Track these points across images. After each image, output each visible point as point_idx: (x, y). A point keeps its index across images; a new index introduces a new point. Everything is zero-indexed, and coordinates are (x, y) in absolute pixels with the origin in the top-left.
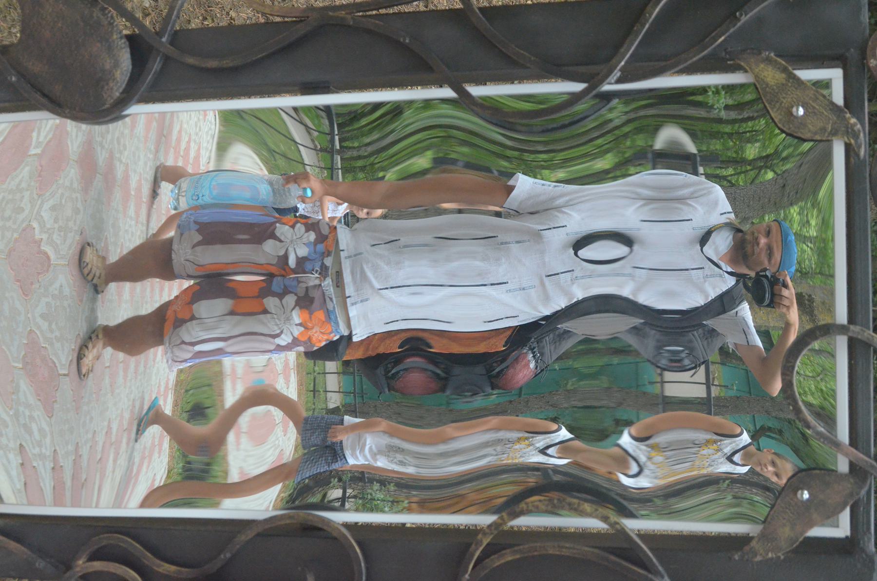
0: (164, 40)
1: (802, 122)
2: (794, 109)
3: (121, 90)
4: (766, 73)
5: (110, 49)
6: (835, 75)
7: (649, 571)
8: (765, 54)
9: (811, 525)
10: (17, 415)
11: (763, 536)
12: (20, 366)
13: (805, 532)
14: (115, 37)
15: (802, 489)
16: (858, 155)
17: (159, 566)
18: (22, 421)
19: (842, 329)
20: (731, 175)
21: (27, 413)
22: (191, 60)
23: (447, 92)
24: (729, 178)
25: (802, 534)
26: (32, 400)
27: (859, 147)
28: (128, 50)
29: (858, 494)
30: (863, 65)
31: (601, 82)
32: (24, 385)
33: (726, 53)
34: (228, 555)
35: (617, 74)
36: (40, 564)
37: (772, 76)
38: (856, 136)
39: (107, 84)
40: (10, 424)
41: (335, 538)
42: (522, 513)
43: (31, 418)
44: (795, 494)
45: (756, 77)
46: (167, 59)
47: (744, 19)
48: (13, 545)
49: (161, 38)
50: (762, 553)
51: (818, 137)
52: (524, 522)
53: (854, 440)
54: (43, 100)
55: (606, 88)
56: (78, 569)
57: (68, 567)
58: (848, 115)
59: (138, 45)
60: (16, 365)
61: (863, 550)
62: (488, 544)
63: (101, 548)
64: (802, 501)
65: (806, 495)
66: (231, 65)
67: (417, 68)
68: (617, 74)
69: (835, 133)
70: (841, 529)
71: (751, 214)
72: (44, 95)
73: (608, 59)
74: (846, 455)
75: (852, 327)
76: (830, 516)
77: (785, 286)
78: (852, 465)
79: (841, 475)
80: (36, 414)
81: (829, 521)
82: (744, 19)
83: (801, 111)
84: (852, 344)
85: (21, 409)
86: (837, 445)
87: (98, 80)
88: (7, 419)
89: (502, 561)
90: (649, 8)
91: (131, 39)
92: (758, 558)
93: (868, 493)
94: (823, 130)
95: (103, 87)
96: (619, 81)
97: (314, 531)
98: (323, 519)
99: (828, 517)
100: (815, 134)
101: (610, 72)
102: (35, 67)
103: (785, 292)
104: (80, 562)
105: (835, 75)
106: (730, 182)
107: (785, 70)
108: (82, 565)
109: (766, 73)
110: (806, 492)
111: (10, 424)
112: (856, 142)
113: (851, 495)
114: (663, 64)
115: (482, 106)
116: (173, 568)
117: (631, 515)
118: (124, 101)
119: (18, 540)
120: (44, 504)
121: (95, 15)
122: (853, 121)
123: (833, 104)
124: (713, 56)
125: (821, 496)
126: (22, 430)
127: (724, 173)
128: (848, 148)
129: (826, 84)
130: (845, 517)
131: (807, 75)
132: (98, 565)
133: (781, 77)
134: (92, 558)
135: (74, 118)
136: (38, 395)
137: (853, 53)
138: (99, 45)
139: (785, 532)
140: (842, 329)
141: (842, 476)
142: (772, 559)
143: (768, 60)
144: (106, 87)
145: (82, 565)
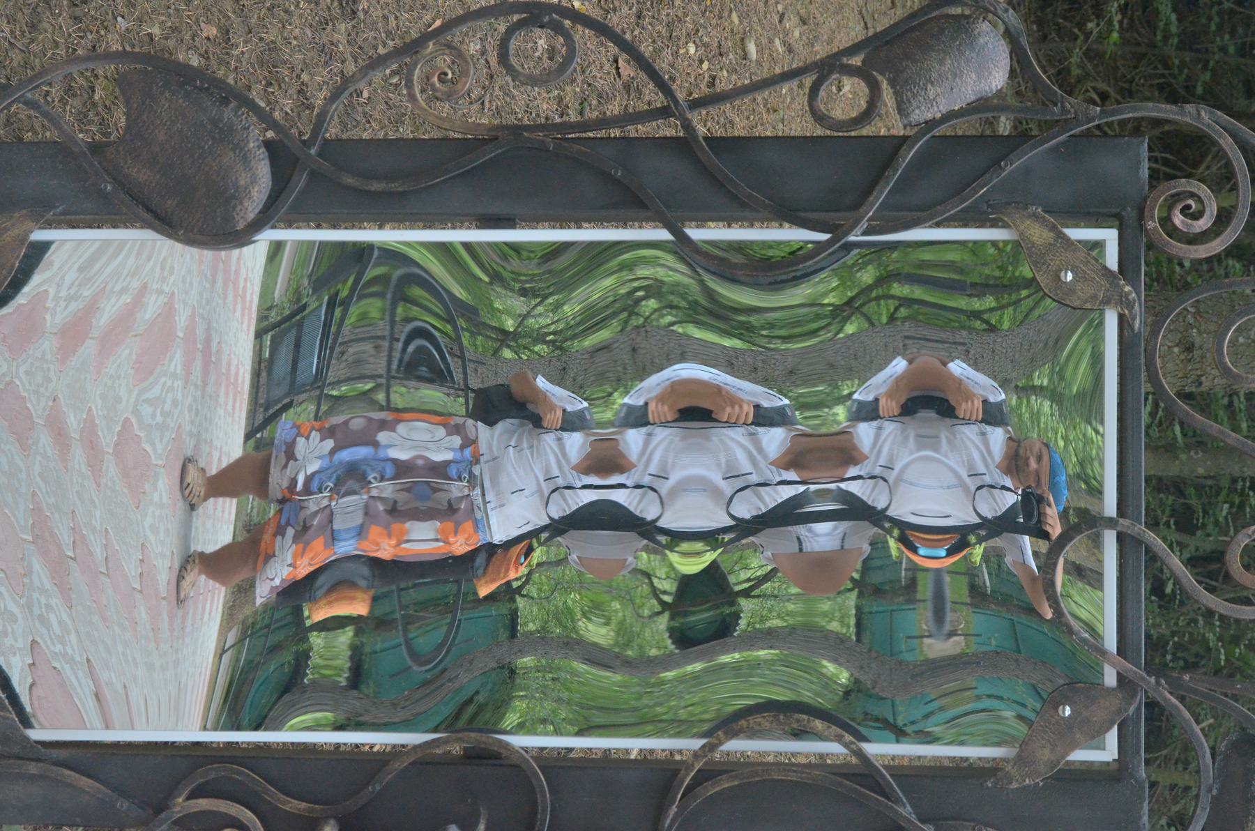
0: (313, 151)
1: (1070, 289)
2: (1063, 274)
3: (257, 211)
4: (1032, 231)
5: (245, 160)
6: (1109, 236)
7: (889, 799)
8: (1032, 209)
9: (1074, 746)
10: (29, 607)
11: (1020, 760)
12: (31, 539)
13: (1067, 754)
14: (252, 145)
15: (1064, 705)
16: (1132, 329)
17: (284, 803)
18: (36, 611)
19: (1111, 523)
20: (991, 310)
21: (43, 601)
22: (349, 181)
23: (664, 235)
24: (985, 316)
25: (1063, 757)
26: (48, 584)
27: (1134, 319)
28: (267, 162)
29: (1126, 710)
30: (1141, 226)
31: (847, 233)
32: (37, 565)
33: (989, 206)
34: (378, 787)
35: (864, 224)
36: (123, 805)
37: (1038, 234)
38: (1130, 306)
39: (241, 203)
40: (19, 615)
41: (516, 766)
42: (416, 748)
43: (48, 606)
44: (1056, 708)
45: (1021, 234)
46: (313, 174)
47: (1009, 169)
48: (84, 782)
49: (309, 148)
50: (1020, 781)
51: (1088, 306)
52: (735, 745)
53: (1121, 651)
54: (141, 211)
55: (852, 238)
56: (178, 809)
57: (161, 807)
58: (1122, 282)
59: (281, 156)
60: (25, 537)
61: (1132, 776)
62: (699, 771)
63: (207, 783)
64: (1064, 718)
65: (1068, 711)
66: (400, 189)
67: (629, 202)
68: (864, 224)
69: (1107, 302)
70: (1107, 751)
71: (1015, 374)
72: (149, 210)
73: (856, 206)
74: (1113, 665)
75: (1121, 521)
76: (1095, 737)
77: (1049, 505)
78: (1120, 677)
79: (1108, 688)
80: (53, 602)
81: (1095, 741)
82: (1009, 169)
83: (1070, 276)
84: (1120, 538)
85: (35, 595)
86: (1103, 653)
87: (229, 198)
88: (16, 610)
89: (717, 789)
90: (902, 151)
91: (268, 144)
92: (1014, 785)
93: (1139, 709)
94: (1095, 297)
95: (234, 208)
96: (865, 233)
97: (488, 758)
98: (500, 741)
99: (1093, 738)
100: (1086, 301)
101: (856, 223)
102: (140, 174)
103: (1049, 511)
104: (180, 800)
105: (1109, 236)
106: (987, 322)
107: (1053, 228)
108: (182, 805)
109: (1032, 231)
110: (1068, 708)
111: (19, 615)
112: (1130, 312)
113: (1119, 712)
114: (917, 214)
115: (707, 255)
116: (304, 805)
117: (867, 740)
118: (257, 225)
119: (90, 776)
120: (84, 727)
121: (226, 116)
122: (1127, 288)
123: (1105, 268)
124: (973, 208)
125: (1085, 713)
126: (37, 623)
127: (977, 304)
128: (1121, 318)
129: (1099, 245)
130: (1112, 737)
131: (1077, 234)
132: (203, 804)
133: (1048, 236)
134: (192, 796)
135: (189, 242)
136: (53, 578)
137: (1130, 213)
138: (231, 153)
139: (1045, 755)
140: (1111, 523)
141: (1109, 690)
142: (1029, 786)
143: (1035, 216)
144: (239, 207)
145: (182, 805)
